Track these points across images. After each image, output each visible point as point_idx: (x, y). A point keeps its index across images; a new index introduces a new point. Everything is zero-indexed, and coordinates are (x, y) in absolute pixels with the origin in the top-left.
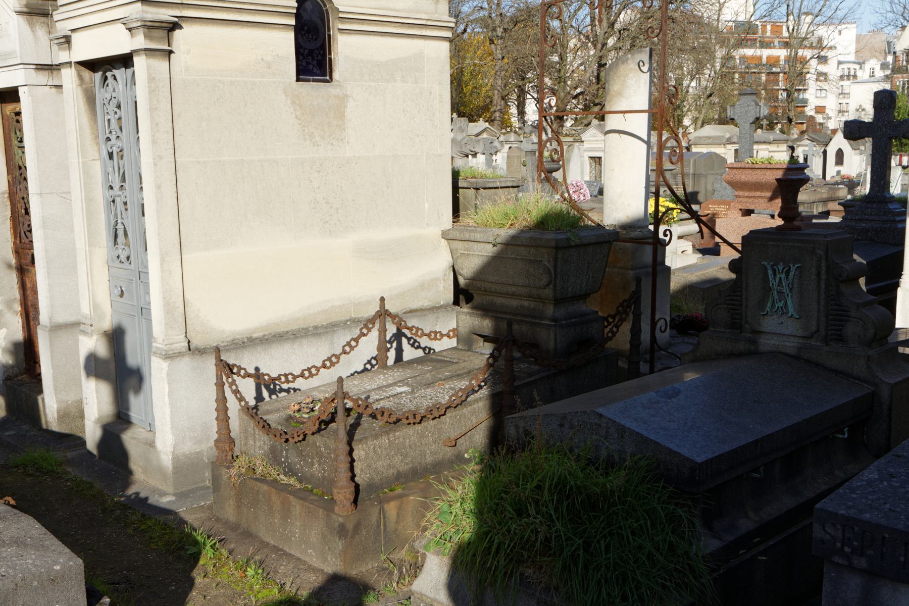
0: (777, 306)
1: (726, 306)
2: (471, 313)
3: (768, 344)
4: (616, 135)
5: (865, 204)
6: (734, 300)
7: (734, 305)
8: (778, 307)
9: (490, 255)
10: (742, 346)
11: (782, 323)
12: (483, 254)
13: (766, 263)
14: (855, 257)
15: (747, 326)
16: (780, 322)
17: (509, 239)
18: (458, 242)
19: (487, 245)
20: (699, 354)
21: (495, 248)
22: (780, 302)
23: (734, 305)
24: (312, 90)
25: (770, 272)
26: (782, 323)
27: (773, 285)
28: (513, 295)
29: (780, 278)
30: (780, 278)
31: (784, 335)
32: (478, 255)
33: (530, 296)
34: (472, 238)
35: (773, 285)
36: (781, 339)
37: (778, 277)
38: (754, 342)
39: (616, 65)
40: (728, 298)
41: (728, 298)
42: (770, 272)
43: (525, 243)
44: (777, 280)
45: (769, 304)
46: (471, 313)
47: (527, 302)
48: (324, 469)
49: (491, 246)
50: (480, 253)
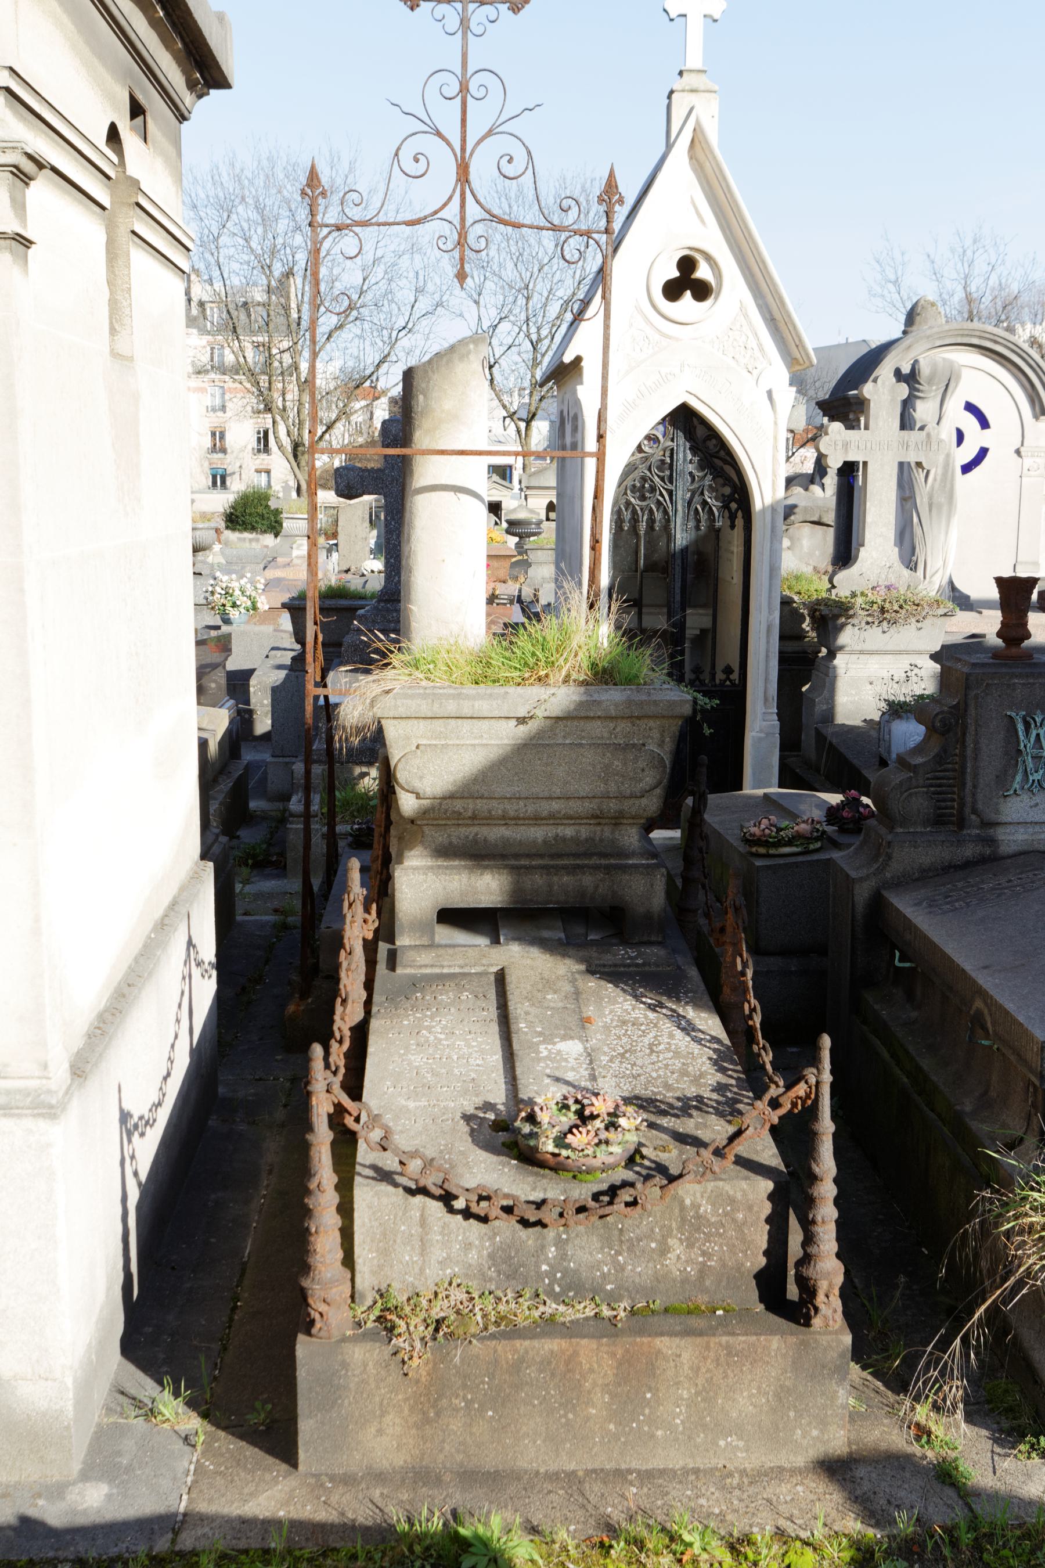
0: (1031, 778)
1: (925, 789)
2: (431, 868)
3: (1014, 841)
4: (449, 495)
5: (382, 604)
6: (938, 779)
7: (940, 786)
8: (1033, 781)
9: (506, 742)
10: (969, 851)
11: (1037, 805)
12: (485, 742)
13: (1013, 714)
14: (804, 689)
15: (973, 817)
16: (1033, 803)
17: (572, 707)
18: (415, 722)
19: (503, 722)
20: (888, 875)
21: (521, 727)
22: (1036, 772)
23: (940, 786)
24: (986, 431)
25: (1020, 727)
26: (1037, 805)
27: (1025, 746)
28: (537, 819)
29: (1038, 735)
30: (1038, 735)
31: (1036, 823)
32: (473, 745)
33: (597, 817)
34: (466, 711)
35: (1025, 746)
36: (1031, 830)
37: (1034, 733)
38: (992, 841)
39: (448, 362)
40: (929, 776)
41: (929, 776)
42: (1020, 727)
43: (613, 713)
44: (1033, 739)
45: (1019, 778)
46: (431, 868)
47: (572, 828)
48: (721, 1235)
49: (514, 722)
50: (477, 742)
